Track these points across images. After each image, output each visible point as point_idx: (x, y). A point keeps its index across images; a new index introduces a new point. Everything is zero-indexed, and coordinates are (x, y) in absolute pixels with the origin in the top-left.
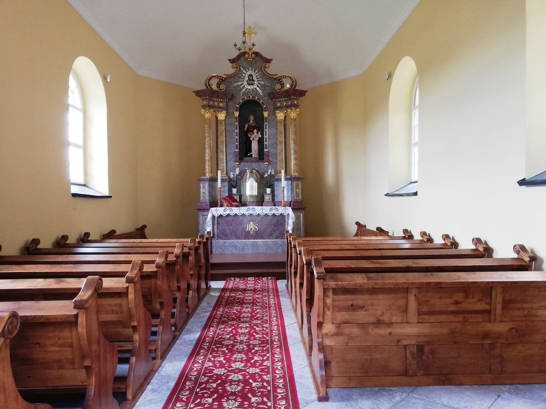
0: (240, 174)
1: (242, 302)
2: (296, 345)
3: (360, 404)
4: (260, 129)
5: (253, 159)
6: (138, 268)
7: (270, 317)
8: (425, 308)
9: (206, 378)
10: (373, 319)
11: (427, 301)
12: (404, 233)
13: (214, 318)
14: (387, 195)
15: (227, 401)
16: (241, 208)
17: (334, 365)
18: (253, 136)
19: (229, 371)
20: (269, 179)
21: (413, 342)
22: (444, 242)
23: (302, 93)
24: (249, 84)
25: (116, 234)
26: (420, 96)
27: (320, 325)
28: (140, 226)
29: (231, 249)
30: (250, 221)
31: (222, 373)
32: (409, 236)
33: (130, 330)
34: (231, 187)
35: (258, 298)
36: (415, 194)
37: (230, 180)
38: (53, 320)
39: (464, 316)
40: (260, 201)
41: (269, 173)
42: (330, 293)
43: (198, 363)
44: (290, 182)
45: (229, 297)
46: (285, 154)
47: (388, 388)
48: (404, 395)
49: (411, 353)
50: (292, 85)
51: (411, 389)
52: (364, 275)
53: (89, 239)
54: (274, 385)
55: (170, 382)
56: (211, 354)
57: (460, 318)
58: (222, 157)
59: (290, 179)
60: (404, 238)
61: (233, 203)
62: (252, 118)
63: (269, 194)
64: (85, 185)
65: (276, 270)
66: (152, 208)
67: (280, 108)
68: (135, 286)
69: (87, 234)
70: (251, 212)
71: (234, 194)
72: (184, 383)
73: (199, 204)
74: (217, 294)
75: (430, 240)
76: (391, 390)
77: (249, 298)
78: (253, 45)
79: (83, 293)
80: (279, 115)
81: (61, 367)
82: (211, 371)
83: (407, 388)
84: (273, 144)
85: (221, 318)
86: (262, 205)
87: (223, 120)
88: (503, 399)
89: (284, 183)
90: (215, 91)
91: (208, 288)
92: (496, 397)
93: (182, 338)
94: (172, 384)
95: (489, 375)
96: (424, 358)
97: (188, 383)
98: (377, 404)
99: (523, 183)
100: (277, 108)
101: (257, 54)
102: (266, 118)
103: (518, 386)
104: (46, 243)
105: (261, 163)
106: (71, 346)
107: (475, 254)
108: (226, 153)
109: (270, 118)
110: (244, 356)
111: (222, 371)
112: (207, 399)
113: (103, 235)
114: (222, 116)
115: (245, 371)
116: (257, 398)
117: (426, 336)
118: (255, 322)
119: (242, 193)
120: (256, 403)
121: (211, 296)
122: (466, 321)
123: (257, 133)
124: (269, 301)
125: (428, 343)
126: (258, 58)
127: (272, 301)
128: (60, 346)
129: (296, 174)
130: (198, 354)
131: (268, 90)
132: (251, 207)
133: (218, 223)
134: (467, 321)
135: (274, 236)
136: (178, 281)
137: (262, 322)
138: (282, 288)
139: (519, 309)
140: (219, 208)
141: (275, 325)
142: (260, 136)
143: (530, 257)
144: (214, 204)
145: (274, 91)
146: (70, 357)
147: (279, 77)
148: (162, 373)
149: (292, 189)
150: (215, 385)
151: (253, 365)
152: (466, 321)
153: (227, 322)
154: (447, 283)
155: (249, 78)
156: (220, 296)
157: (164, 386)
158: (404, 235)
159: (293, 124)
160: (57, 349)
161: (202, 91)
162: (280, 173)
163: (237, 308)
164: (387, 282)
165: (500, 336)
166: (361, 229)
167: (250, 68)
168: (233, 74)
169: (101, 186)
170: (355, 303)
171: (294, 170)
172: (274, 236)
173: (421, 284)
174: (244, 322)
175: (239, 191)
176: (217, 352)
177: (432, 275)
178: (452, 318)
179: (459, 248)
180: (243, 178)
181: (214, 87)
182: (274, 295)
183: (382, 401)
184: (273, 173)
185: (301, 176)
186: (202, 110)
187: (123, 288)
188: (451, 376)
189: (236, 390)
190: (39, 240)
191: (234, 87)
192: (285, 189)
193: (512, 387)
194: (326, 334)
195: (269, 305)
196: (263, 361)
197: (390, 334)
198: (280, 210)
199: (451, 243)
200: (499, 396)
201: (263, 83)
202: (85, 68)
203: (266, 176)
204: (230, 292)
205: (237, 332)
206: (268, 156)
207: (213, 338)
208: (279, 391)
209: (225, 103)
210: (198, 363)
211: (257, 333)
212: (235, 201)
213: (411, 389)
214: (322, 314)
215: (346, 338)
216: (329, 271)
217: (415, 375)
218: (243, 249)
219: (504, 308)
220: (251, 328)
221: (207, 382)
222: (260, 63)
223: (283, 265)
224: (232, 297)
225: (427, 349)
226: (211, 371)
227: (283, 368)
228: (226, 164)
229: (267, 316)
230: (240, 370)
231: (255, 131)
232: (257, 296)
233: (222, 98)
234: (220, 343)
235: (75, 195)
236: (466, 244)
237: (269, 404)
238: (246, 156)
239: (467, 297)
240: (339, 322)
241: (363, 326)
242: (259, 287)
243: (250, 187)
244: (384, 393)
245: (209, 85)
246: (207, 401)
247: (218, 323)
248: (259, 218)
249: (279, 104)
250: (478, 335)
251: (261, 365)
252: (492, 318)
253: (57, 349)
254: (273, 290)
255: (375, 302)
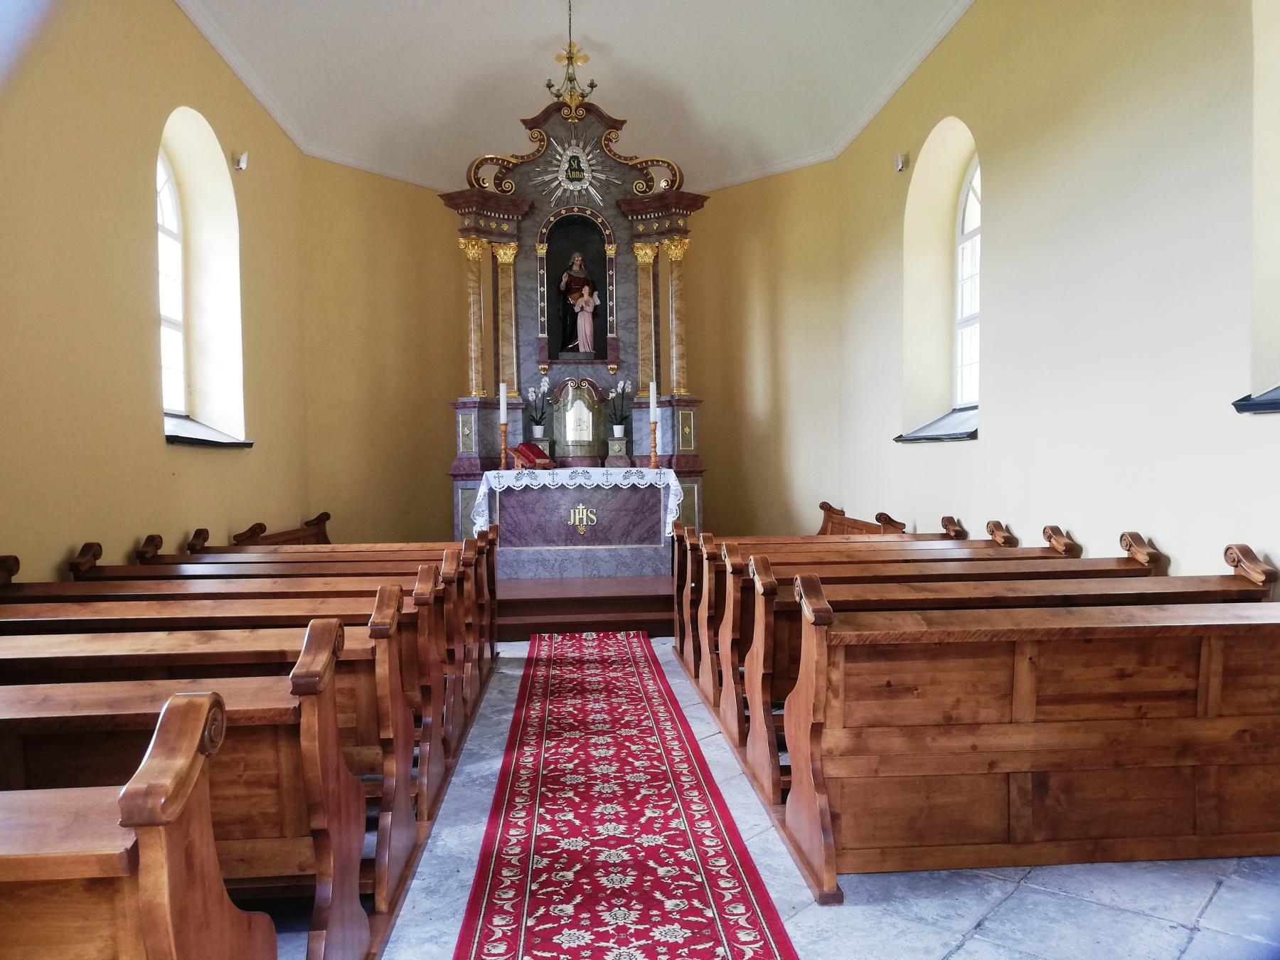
0: (551, 390)
1: (581, 689)
2: (733, 782)
3: (915, 908)
4: (598, 284)
5: (579, 357)
6: (394, 604)
7: (657, 721)
8: (1051, 690)
9: (546, 861)
10: (935, 717)
11: (1057, 673)
12: (945, 526)
13: (526, 725)
14: (899, 439)
15: (610, 909)
16: (556, 471)
17: (846, 821)
18: (581, 302)
19: (594, 843)
20: (618, 402)
21: (1026, 767)
22: (1047, 544)
23: (696, 202)
24: (571, 180)
25: (267, 533)
26: (985, 201)
27: (817, 730)
28: (313, 515)
29: (533, 567)
30: (579, 503)
31: (580, 849)
32: (956, 532)
33: (377, 750)
34: (530, 421)
35: (617, 679)
36: (973, 435)
37: (527, 407)
38: (242, 723)
39: (1138, 705)
40: (598, 455)
41: (619, 390)
42: (840, 657)
43: (516, 826)
44: (669, 411)
45: (547, 677)
46: (657, 344)
47: (969, 872)
48: (1010, 887)
49: (1022, 791)
50: (673, 182)
51: (1021, 874)
52: (916, 615)
53: (207, 544)
54: (708, 872)
55: (462, 872)
56: (541, 805)
57: (1129, 709)
58: (509, 351)
59: (670, 403)
60: (945, 537)
61: (538, 461)
62: (577, 259)
63: (619, 439)
64: (187, 417)
65: (650, 614)
66: (342, 471)
67: (643, 237)
68: (390, 645)
69: (202, 534)
70: (580, 480)
71: (538, 440)
72: (497, 872)
73: (455, 463)
74: (520, 672)
75: (1011, 541)
76: (977, 876)
77: (594, 679)
78: (592, 86)
79: (309, 659)
80: (641, 253)
81: (252, 835)
82: (553, 845)
83: (1011, 871)
84: (630, 321)
85: (541, 726)
86: (603, 466)
87: (509, 264)
88: (1231, 888)
89: (655, 413)
90: (492, 195)
91: (495, 656)
92: (1214, 885)
93: (461, 772)
94: (469, 875)
95: (1192, 837)
96: (1049, 802)
97: (505, 872)
98: (953, 907)
99: (1245, 405)
100: (638, 237)
101: (590, 109)
102: (611, 259)
103: (1257, 860)
104: (113, 557)
105: (600, 367)
106: (276, 785)
107: (1128, 569)
108: (517, 341)
109: (620, 259)
110: (619, 809)
111: (577, 844)
112: (560, 907)
113: (235, 537)
114: (506, 254)
115: (631, 841)
116: (677, 901)
117: (1055, 752)
118: (624, 732)
119: (557, 436)
120: (678, 912)
121: (506, 676)
122: (1141, 716)
123: (591, 295)
124: (644, 687)
125: (1058, 767)
126: (592, 118)
127: (651, 687)
128: (249, 784)
129: (683, 391)
130: (512, 806)
131: (616, 194)
132: (580, 469)
133: (502, 507)
134: (1143, 717)
135: (635, 535)
136: (450, 639)
137: (642, 732)
138: (666, 654)
139: (1256, 688)
140: (503, 472)
141: (673, 739)
142: (598, 302)
143: (1266, 573)
144: (491, 462)
145: (629, 197)
146: (273, 810)
147: (641, 163)
148: (438, 851)
149: (673, 426)
150: (570, 875)
151: (648, 828)
152: (1141, 716)
153: (559, 735)
154: (1107, 630)
155: (571, 165)
156: (525, 677)
157: (450, 881)
158: (944, 531)
159: (675, 274)
160: (242, 791)
161: (461, 193)
162: (647, 388)
163: (573, 702)
164: (974, 628)
165: (1216, 748)
166: (834, 518)
167: (573, 142)
168: (533, 154)
169: (226, 418)
170: (894, 679)
171: (678, 383)
172: (635, 535)
173: (1050, 632)
174: (597, 733)
175: (548, 432)
176: (554, 801)
177: (1070, 613)
178: (1112, 710)
179: (1083, 556)
180: (557, 402)
181: (489, 185)
182: (651, 672)
183: (962, 899)
184: (628, 390)
185: (695, 397)
186: (462, 240)
187: (365, 651)
188: (1110, 841)
189: (624, 885)
190: (99, 545)
191: (535, 186)
192: (659, 425)
193: (1244, 862)
194: (830, 752)
195: (646, 693)
196: (668, 819)
197: (974, 748)
198: (649, 476)
199: (1066, 545)
200: (1220, 883)
201: (603, 177)
202: (189, 136)
203: (612, 395)
204: (548, 666)
205: (587, 754)
206: (617, 349)
207: (536, 769)
208: (722, 883)
209: (515, 225)
210: (516, 826)
211: (637, 758)
212: (540, 454)
213: (1020, 872)
214: (822, 706)
215: (874, 759)
216: (839, 606)
217: (1028, 841)
218: (562, 568)
219: (1225, 686)
220: (620, 746)
221: (549, 869)
222: (597, 129)
223: (665, 602)
224: (554, 677)
225: (1054, 781)
226: (553, 845)
227: (717, 833)
228: (518, 367)
229: (648, 718)
230: (617, 842)
231: (586, 290)
232: (612, 674)
233: (506, 211)
234: (556, 780)
235: (172, 440)
236: (1101, 546)
237: (709, 913)
238: (564, 348)
239: (1144, 663)
240: (857, 724)
241: (912, 731)
242: (611, 653)
243: (576, 423)
244: (964, 882)
245: (477, 180)
246: (561, 910)
247: (540, 737)
248: (598, 496)
249: (641, 228)
250: (1167, 748)
251: (665, 827)
252: (1200, 708)
253: (242, 791)
254: (647, 661)
255: (940, 676)
